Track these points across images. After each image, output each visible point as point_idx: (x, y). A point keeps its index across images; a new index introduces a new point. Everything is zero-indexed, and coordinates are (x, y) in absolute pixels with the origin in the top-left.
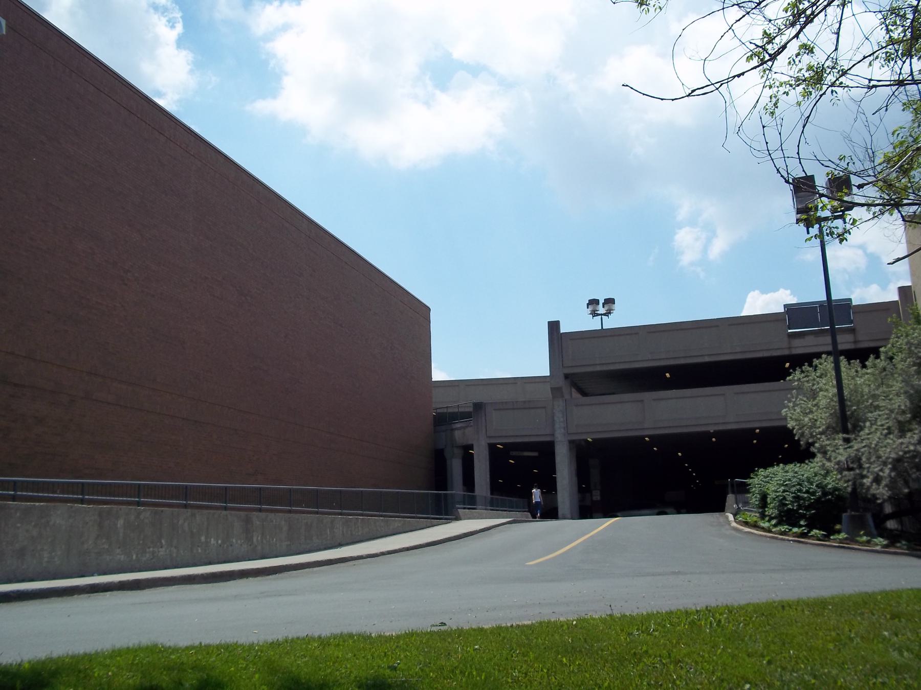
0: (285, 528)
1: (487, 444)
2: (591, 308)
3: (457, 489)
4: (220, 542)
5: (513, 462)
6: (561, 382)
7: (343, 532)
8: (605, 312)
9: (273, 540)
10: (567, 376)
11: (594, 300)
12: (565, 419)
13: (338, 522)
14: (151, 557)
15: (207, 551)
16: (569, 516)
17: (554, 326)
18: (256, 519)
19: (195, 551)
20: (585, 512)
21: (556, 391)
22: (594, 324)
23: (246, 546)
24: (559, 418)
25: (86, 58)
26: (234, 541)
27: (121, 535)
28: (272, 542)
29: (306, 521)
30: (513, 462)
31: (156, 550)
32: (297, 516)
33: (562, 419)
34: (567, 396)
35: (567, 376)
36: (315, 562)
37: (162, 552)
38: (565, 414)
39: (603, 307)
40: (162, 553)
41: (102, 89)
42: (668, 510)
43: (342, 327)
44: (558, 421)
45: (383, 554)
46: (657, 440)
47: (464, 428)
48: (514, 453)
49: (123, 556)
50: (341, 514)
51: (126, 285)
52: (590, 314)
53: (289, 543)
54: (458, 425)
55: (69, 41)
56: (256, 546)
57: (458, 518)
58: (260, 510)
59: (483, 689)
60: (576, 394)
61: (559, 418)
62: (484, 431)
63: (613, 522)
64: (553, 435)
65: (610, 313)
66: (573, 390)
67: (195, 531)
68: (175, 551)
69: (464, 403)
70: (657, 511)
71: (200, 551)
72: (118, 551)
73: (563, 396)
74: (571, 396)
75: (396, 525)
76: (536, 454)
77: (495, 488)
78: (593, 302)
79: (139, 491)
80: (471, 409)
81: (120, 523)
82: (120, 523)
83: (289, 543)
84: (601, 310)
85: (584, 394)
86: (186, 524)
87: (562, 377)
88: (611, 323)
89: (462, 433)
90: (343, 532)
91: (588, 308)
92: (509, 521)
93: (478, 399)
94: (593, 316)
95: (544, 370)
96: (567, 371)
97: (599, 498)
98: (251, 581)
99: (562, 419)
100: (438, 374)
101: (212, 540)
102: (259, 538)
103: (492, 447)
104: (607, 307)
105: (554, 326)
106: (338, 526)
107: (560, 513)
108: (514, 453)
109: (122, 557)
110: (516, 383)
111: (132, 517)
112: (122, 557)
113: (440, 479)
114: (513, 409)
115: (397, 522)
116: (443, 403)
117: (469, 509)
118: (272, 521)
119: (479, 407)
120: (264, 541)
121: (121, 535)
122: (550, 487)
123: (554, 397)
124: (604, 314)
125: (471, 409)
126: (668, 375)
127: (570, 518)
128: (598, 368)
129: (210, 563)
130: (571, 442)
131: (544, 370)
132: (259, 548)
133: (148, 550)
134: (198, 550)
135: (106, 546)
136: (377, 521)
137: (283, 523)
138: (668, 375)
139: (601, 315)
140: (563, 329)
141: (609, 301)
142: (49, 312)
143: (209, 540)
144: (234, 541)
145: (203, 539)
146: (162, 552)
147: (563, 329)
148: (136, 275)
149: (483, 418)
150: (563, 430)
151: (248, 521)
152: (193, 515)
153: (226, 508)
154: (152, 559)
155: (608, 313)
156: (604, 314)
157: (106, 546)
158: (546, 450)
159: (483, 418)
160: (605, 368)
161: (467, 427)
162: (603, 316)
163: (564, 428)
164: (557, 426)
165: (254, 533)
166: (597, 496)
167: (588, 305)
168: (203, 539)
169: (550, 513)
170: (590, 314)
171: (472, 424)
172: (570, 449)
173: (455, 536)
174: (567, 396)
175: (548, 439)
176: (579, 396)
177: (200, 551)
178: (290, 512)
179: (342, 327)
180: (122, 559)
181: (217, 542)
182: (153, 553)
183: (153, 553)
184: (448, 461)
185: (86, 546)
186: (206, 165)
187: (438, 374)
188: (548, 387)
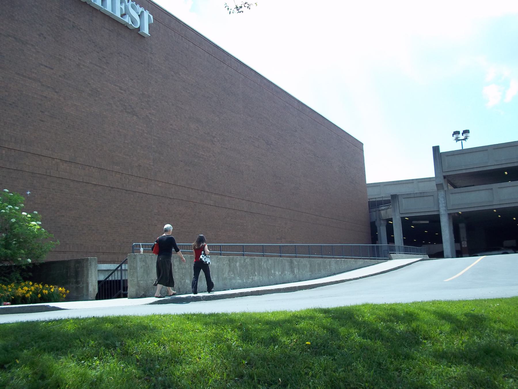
0: (309, 266)
1: (400, 218)
2: (455, 136)
3: (384, 243)
4: (280, 273)
5: (412, 226)
6: (442, 181)
7: (335, 267)
8: (464, 138)
9: (303, 272)
10: (445, 177)
11: (457, 132)
12: (445, 201)
13: (333, 263)
14: (252, 281)
15: (275, 278)
16: (451, 256)
17: (436, 149)
18: (295, 261)
19: (270, 278)
20: (459, 254)
21: (439, 186)
22: (457, 146)
23: (291, 275)
24: (442, 201)
25: (188, 29)
26: (286, 272)
27: (239, 270)
28: (303, 273)
29: (318, 262)
30: (412, 226)
31: (253, 277)
32: (313, 259)
33: (443, 202)
34: (446, 189)
35: (445, 177)
36: (330, 282)
37: (256, 278)
38: (445, 199)
39: (463, 135)
40: (256, 279)
41: (196, 44)
42: (509, 252)
43: (318, 157)
44: (441, 203)
45: (360, 278)
46: (500, 211)
47: (387, 209)
48: (414, 222)
49: (240, 280)
50: (333, 258)
51: (214, 144)
52: (455, 140)
53: (311, 273)
54: (383, 208)
55: (180, 22)
56: (296, 275)
57: (390, 259)
58: (296, 257)
59: (327, 388)
60: (450, 187)
61: (442, 201)
62: (398, 211)
63: (482, 259)
64: (439, 211)
65: (467, 138)
66: (449, 184)
67: (269, 268)
68: (261, 278)
69: (385, 194)
70: (502, 252)
71: (272, 278)
72: (238, 278)
73: (443, 189)
74: (448, 189)
75: (360, 263)
76: (428, 222)
77: (406, 242)
78: (456, 133)
79: (243, 248)
80: (390, 198)
81: (238, 264)
82: (238, 264)
83: (311, 273)
84: (461, 137)
85: (455, 187)
86: (265, 264)
87: (442, 178)
88: (468, 145)
89: (385, 212)
90: (335, 267)
91: (453, 136)
92: (421, 259)
93: (393, 192)
94: (457, 141)
95: (431, 174)
96: (445, 174)
97: (466, 246)
98: (304, 291)
99: (443, 202)
100: (370, 179)
101: (277, 272)
102: (297, 271)
103: (403, 219)
104: (465, 135)
105: (436, 149)
106: (333, 264)
107: (445, 255)
108: (414, 222)
109: (240, 281)
110: (413, 182)
111: (242, 261)
112: (240, 281)
113: (374, 238)
114: (415, 197)
115: (360, 262)
116: (373, 195)
117: (354, 259)
118: (302, 262)
119: (394, 197)
120: (300, 273)
121: (239, 270)
122: (439, 240)
123: (438, 190)
124: (463, 140)
125: (390, 198)
126: (506, 173)
127: (451, 257)
128: (464, 172)
129: (277, 284)
130: (449, 214)
131: (431, 174)
132: (298, 276)
133: (250, 277)
134: (271, 278)
135: (233, 276)
136: (351, 262)
137: (307, 263)
138: (506, 173)
139: (462, 140)
140: (442, 150)
141: (466, 132)
142: (182, 161)
143: (275, 272)
144: (286, 272)
145: (273, 271)
146: (256, 278)
147: (442, 150)
148: (218, 138)
149: (397, 203)
150: (444, 208)
151: (291, 262)
152: (268, 260)
153: (281, 256)
154: (252, 282)
155: (465, 139)
156: (463, 140)
157: (233, 276)
158: (435, 220)
159: (397, 203)
160: (468, 171)
161: (388, 208)
162: (462, 141)
163: (445, 207)
164: (441, 206)
165: (295, 269)
166: (465, 244)
167: (453, 135)
168: (273, 271)
169: (440, 255)
170: (455, 140)
171: (391, 207)
172: (449, 219)
173: (394, 268)
174: (446, 189)
175: (436, 213)
176: (452, 188)
177: (272, 278)
178: (309, 257)
179: (318, 157)
180: (240, 282)
181: (279, 273)
182: (252, 279)
183: (252, 279)
184: (378, 228)
185: (225, 276)
186: (246, 77)
187: (370, 179)
188: (434, 184)
